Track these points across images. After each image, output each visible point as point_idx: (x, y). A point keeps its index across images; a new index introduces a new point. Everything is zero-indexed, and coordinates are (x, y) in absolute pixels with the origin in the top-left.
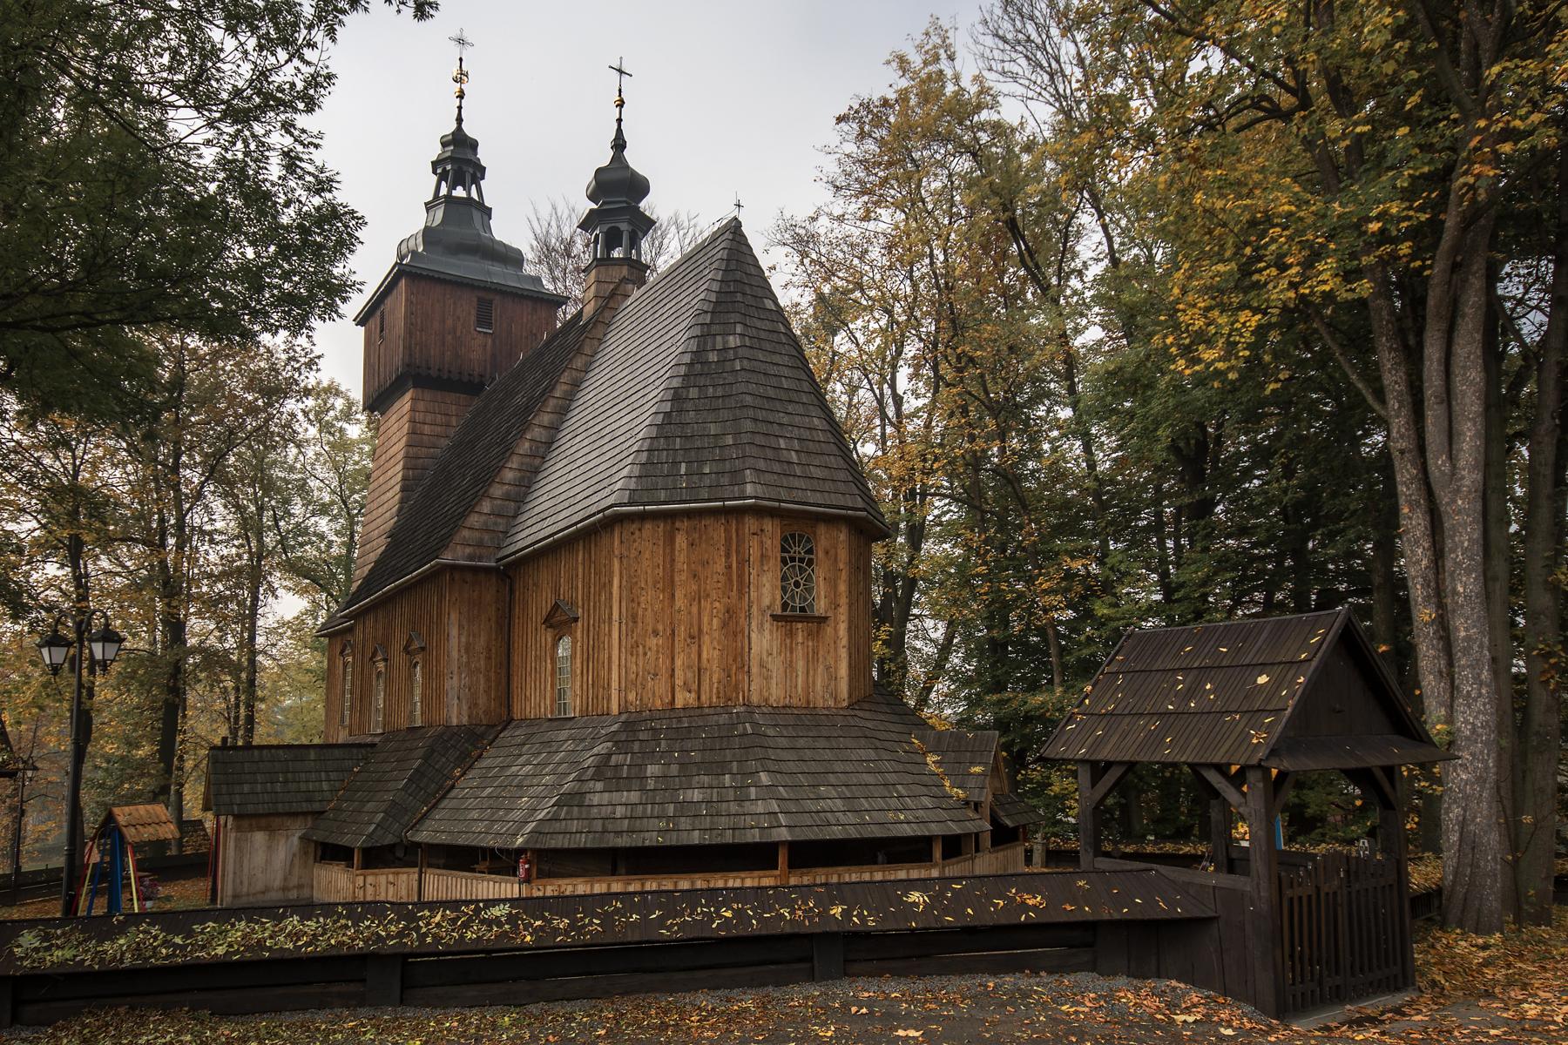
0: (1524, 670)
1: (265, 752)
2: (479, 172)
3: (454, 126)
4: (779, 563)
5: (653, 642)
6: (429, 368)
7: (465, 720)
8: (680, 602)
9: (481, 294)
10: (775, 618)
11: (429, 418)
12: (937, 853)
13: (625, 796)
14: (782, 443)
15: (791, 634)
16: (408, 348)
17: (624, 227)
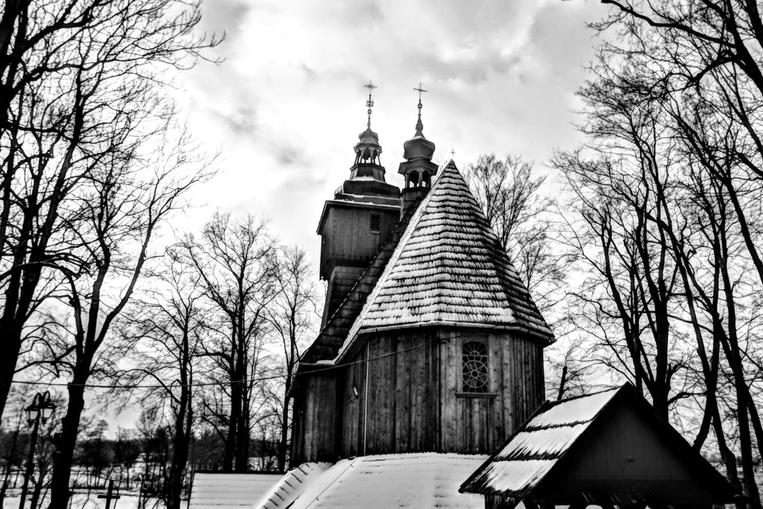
0: (170, 438)
3: (367, 127)
5: (384, 411)
6: (343, 255)
8: (399, 387)
9: (373, 212)
10: (458, 396)
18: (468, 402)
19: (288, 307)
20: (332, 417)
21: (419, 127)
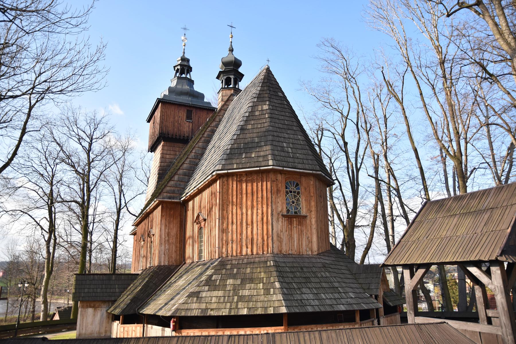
1: (95, 276)
2: (189, 69)
4: (285, 193)
7: (166, 264)
11: (169, 152)
12: (358, 318)
13: (215, 293)
14: (285, 145)
15: (291, 223)
16: (161, 127)
17: (232, 77)
18: (290, 220)
19: (117, 173)
20: (177, 235)
21: (231, 50)
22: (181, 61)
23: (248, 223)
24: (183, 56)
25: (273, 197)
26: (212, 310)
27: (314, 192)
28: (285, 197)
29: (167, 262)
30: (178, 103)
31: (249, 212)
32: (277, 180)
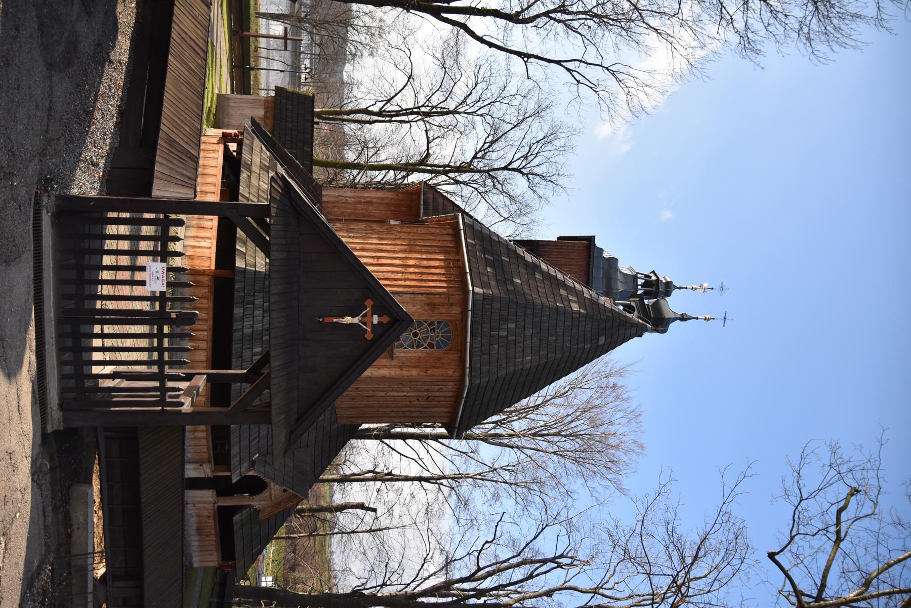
21: (683, 318)
22: (664, 281)
23: (380, 260)
24: (675, 287)
25: (423, 297)
26: (249, 177)
27: (434, 375)
28: (424, 318)
29: (326, 201)
30: (591, 270)
31: (397, 262)
32: (452, 305)
